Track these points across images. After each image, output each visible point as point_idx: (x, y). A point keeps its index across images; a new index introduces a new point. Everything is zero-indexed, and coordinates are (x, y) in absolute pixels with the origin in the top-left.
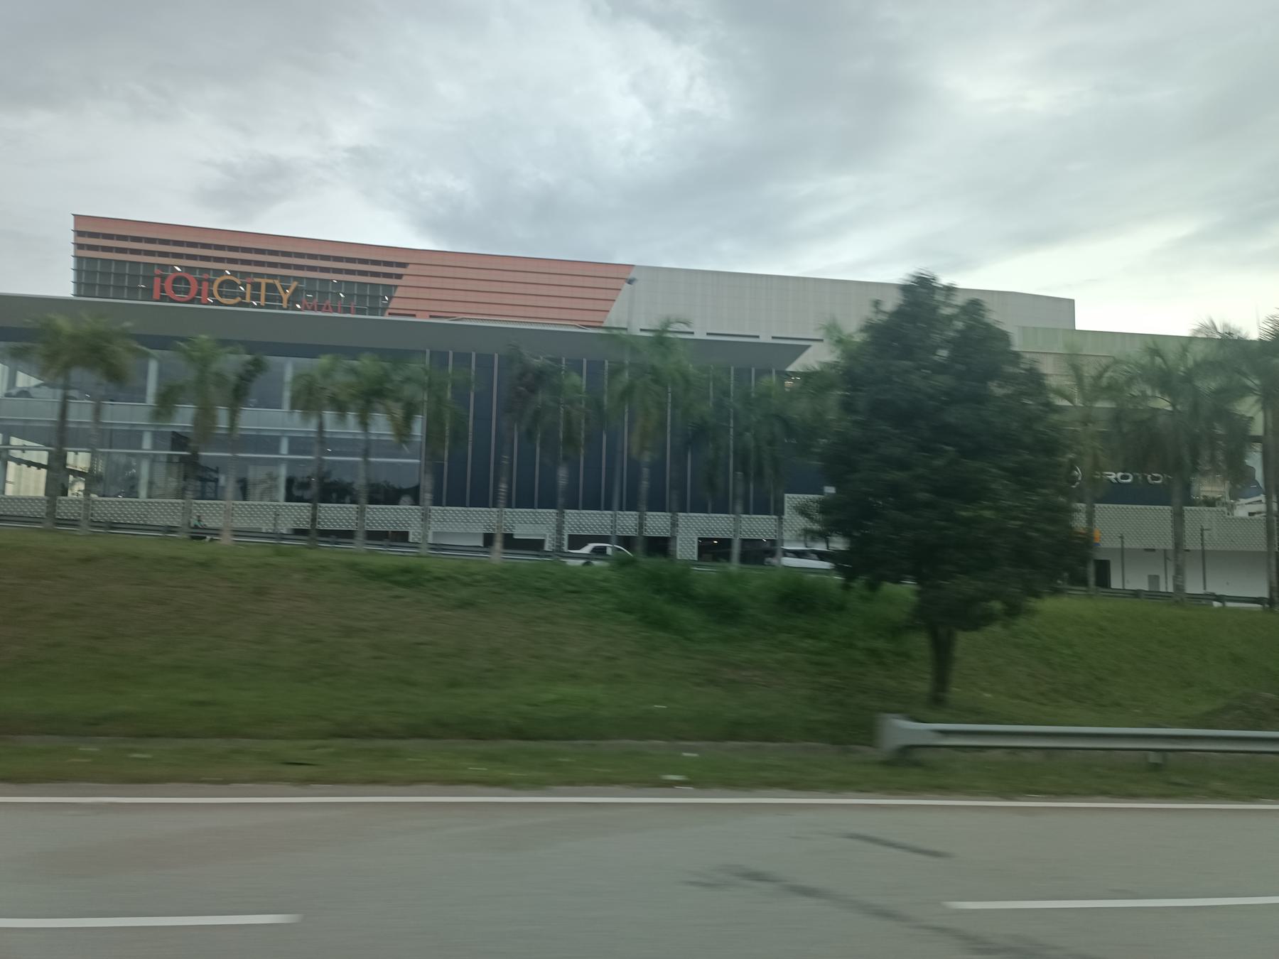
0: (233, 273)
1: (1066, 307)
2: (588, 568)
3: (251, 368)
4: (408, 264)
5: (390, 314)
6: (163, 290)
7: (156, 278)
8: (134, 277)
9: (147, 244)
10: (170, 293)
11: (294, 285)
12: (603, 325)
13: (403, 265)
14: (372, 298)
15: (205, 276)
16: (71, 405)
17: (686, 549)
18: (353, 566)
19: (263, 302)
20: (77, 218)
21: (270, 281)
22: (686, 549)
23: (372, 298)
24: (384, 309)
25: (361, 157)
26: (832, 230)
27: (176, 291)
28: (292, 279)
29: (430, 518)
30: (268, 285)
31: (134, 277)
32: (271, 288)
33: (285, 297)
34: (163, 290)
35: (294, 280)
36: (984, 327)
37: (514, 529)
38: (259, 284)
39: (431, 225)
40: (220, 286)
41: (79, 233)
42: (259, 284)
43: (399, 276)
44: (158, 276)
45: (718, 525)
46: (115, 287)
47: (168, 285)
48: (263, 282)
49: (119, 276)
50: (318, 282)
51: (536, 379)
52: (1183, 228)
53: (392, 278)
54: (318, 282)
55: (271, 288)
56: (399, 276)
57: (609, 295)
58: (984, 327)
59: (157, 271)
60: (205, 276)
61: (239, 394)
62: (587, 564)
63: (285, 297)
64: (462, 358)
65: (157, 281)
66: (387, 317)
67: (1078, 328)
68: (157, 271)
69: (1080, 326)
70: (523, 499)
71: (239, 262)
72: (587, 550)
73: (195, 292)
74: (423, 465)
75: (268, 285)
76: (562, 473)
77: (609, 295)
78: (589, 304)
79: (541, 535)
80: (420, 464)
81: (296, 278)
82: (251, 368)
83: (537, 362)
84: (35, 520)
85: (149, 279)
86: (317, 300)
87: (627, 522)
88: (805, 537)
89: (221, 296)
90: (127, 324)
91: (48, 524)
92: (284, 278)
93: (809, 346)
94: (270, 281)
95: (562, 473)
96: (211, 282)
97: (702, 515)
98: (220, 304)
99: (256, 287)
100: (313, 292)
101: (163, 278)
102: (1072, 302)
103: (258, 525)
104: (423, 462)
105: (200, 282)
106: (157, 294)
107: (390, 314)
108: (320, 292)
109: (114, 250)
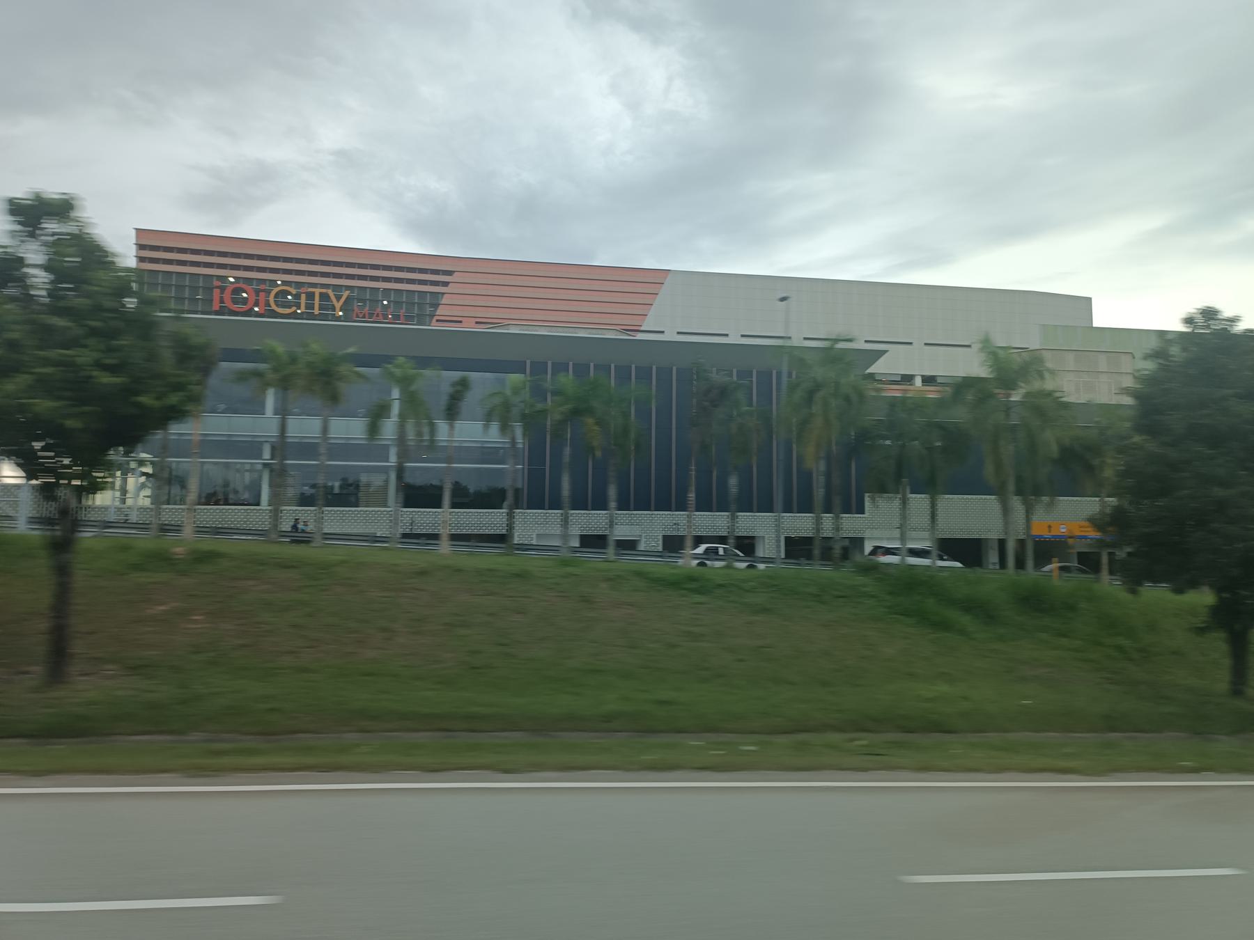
0: (284, 283)
1: (1084, 304)
2: (752, 571)
3: (459, 388)
4: (454, 272)
5: (437, 321)
6: (222, 301)
7: (215, 290)
8: (195, 289)
9: (384, 272)
10: (228, 303)
11: (346, 294)
12: (642, 329)
13: (450, 273)
14: (424, 305)
15: (262, 287)
16: (290, 420)
17: (769, 547)
18: (640, 574)
19: (316, 311)
20: (140, 232)
21: (324, 291)
22: (769, 547)
23: (424, 305)
24: (432, 316)
25: (346, 159)
26: (810, 227)
27: (235, 301)
28: (344, 289)
29: (822, 530)
30: (321, 294)
31: (195, 289)
32: (324, 297)
33: (338, 305)
34: (222, 301)
35: (346, 290)
36: (68, 237)
37: (137, 515)
38: (314, 293)
39: (415, 226)
40: (276, 296)
41: (141, 247)
42: (314, 293)
43: (446, 284)
44: (217, 287)
45: (800, 524)
46: (189, 299)
47: (227, 296)
48: (317, 291)
49: (180, 287)
50: (393, 292)
51: (723, 394)
52: (1154, 220)
53: (378, 281)
54: (428, 294)
55: (324, 297)
56: (446, 284)
57: (647, 299)
58: (68, 237)
59: (216, 283)
60: (262, 287)
61: (452, 412)
62: (702, 564)
63: (338, 305)
64: (644, 373)
65: (216, 292)
66: (435, 326)
67: (1094, 326)
68: (216, 283)
69: (1097, 323)
70: (704, 504)
71: (242, 269)
72: (701, 549)
73: (253, 303)
74: (526, 471)
75: (321, 294)
76: (733, 481)
77: (647, 299)
78: (629, 309)
79: (635, 536)
80: (523, 468)
81: (348, 288)
82: (459, 388)
83: (717, 378)
84: (262, 533)
85: (209, 290)
86: (367, 308)
87: (714, 522)
88: (33, 510)
89: (277, 305)
90: (351, 350)
91: (273, 536)
92: (337, 288)
93: (885, 352)
94: (324, 291)
95: (733, 481)
96: (269, 292)
97: (666, 513)
98: (276, 315)
99: (310, 296)
100: (364, 301)
101: (223, 289)
102: (1089, 300)
103: (372, 531)
104: (526, 467)
105: (257, 292)
106: (216, 306)
107: (437, 321)
108: (360, 302)
109: (381, 279)
